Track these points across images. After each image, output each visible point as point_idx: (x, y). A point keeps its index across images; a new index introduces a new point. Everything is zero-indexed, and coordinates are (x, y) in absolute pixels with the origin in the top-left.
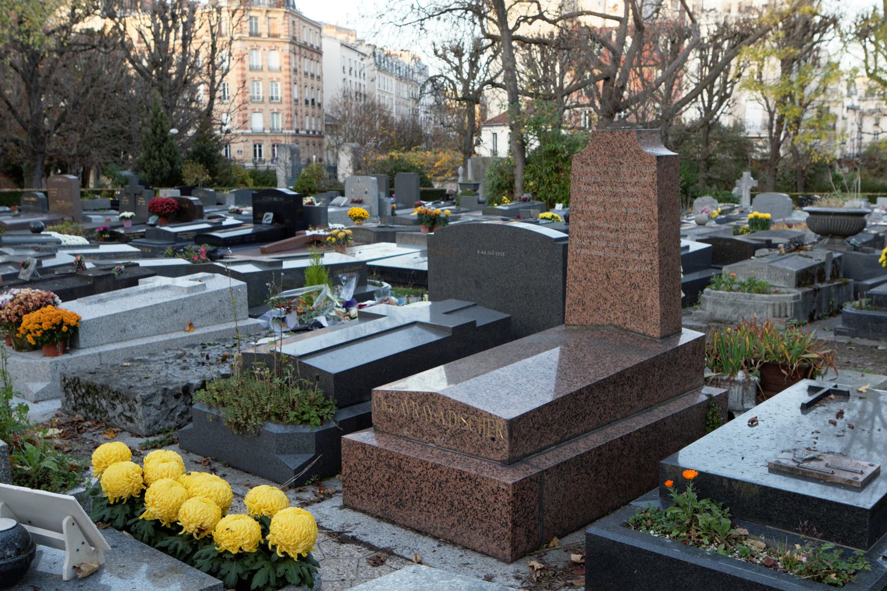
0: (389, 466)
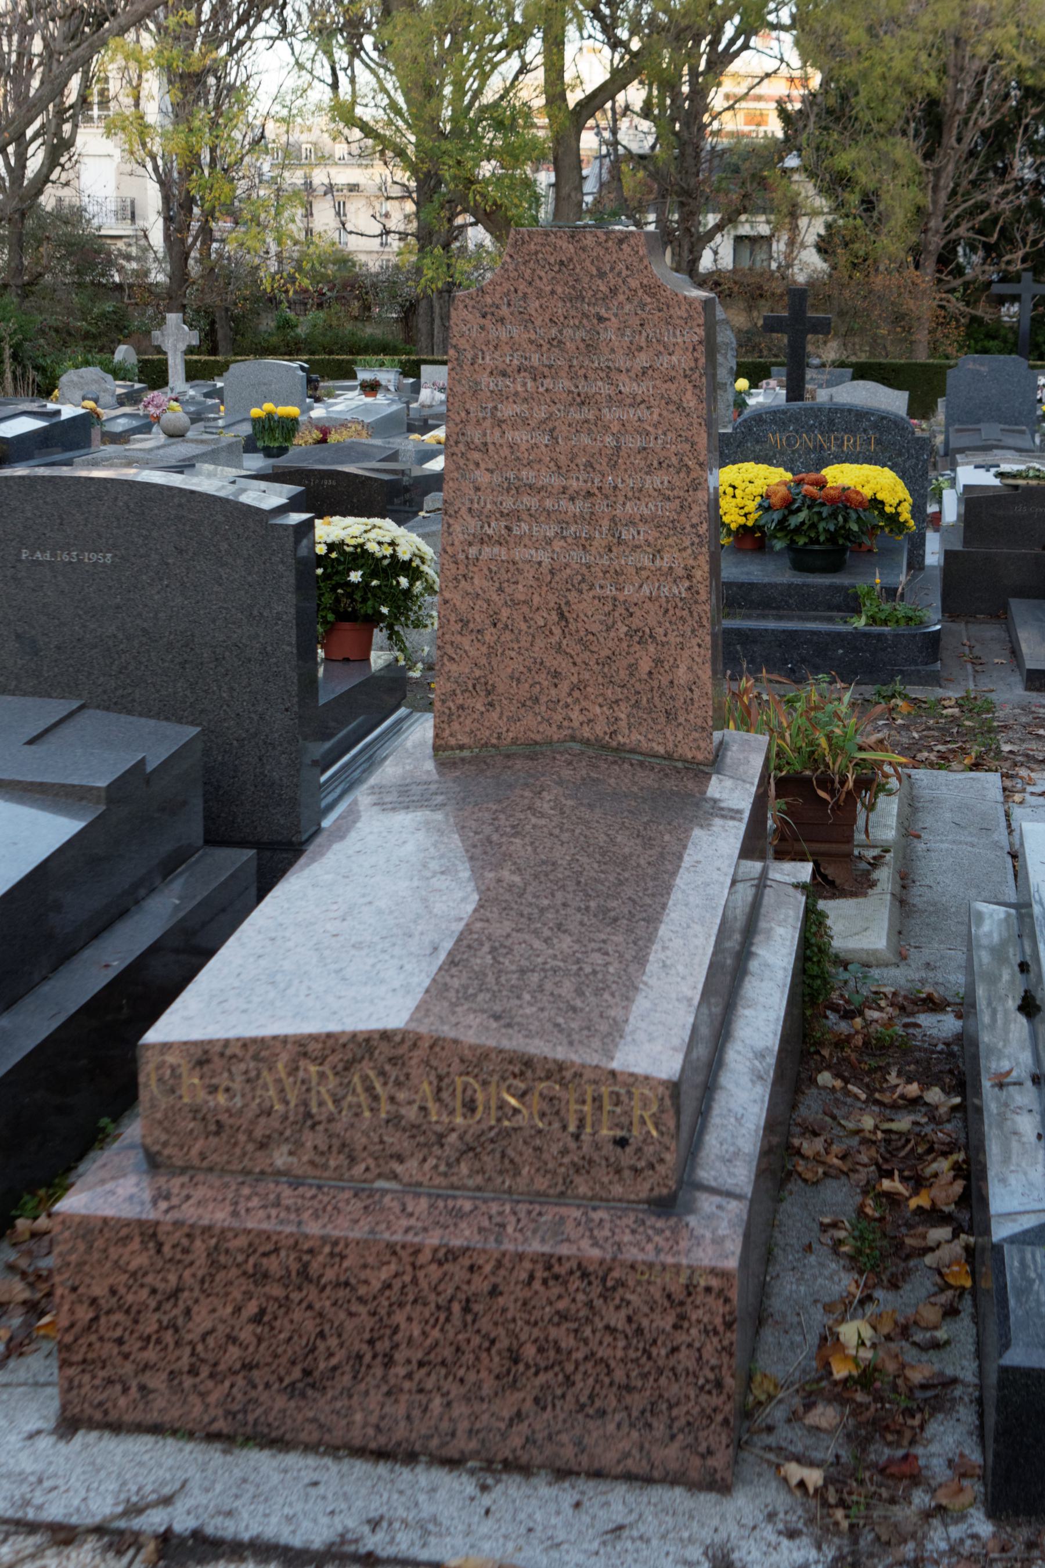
0: (261, 1277)
